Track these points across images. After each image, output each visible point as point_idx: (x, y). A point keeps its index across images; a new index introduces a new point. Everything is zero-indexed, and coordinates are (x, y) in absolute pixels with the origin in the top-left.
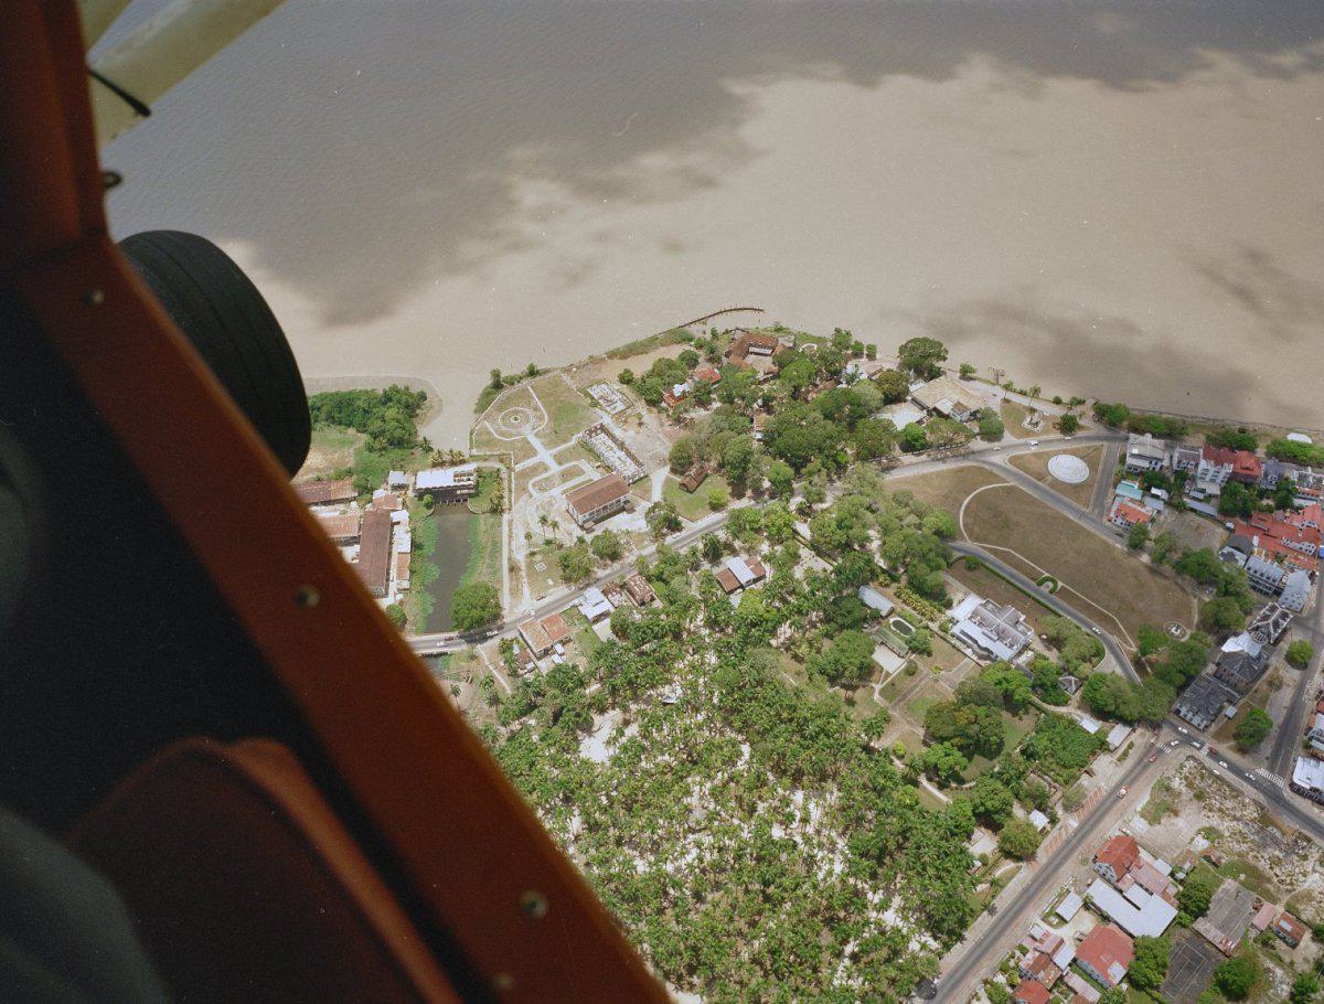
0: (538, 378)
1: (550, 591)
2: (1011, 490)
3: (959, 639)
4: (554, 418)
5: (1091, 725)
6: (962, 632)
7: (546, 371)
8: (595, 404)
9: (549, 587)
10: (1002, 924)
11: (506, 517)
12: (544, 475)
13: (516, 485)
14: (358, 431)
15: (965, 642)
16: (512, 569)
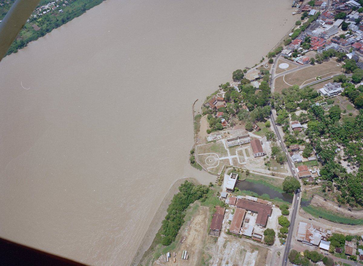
1: (285, 168)
3: (331, 96)
4: (216, 152)
10: (316, 83)
13: (239, 166)
15: (332, 95)
16: (273, 175)
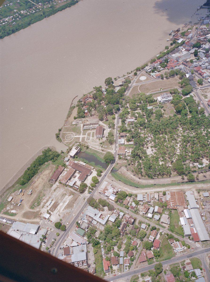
0: (62, 130)
2: (141, 85)
3: (163, 103)
4: (74, 132)
5: (188, 96)
6: (163, 101)
7: (62, 129)
8: (76, 125)
9: (111, 147)
11: (90, 147)
12: (86, 138)
14: (47, 162)
15: (164, 102)
16: (103, 151)
